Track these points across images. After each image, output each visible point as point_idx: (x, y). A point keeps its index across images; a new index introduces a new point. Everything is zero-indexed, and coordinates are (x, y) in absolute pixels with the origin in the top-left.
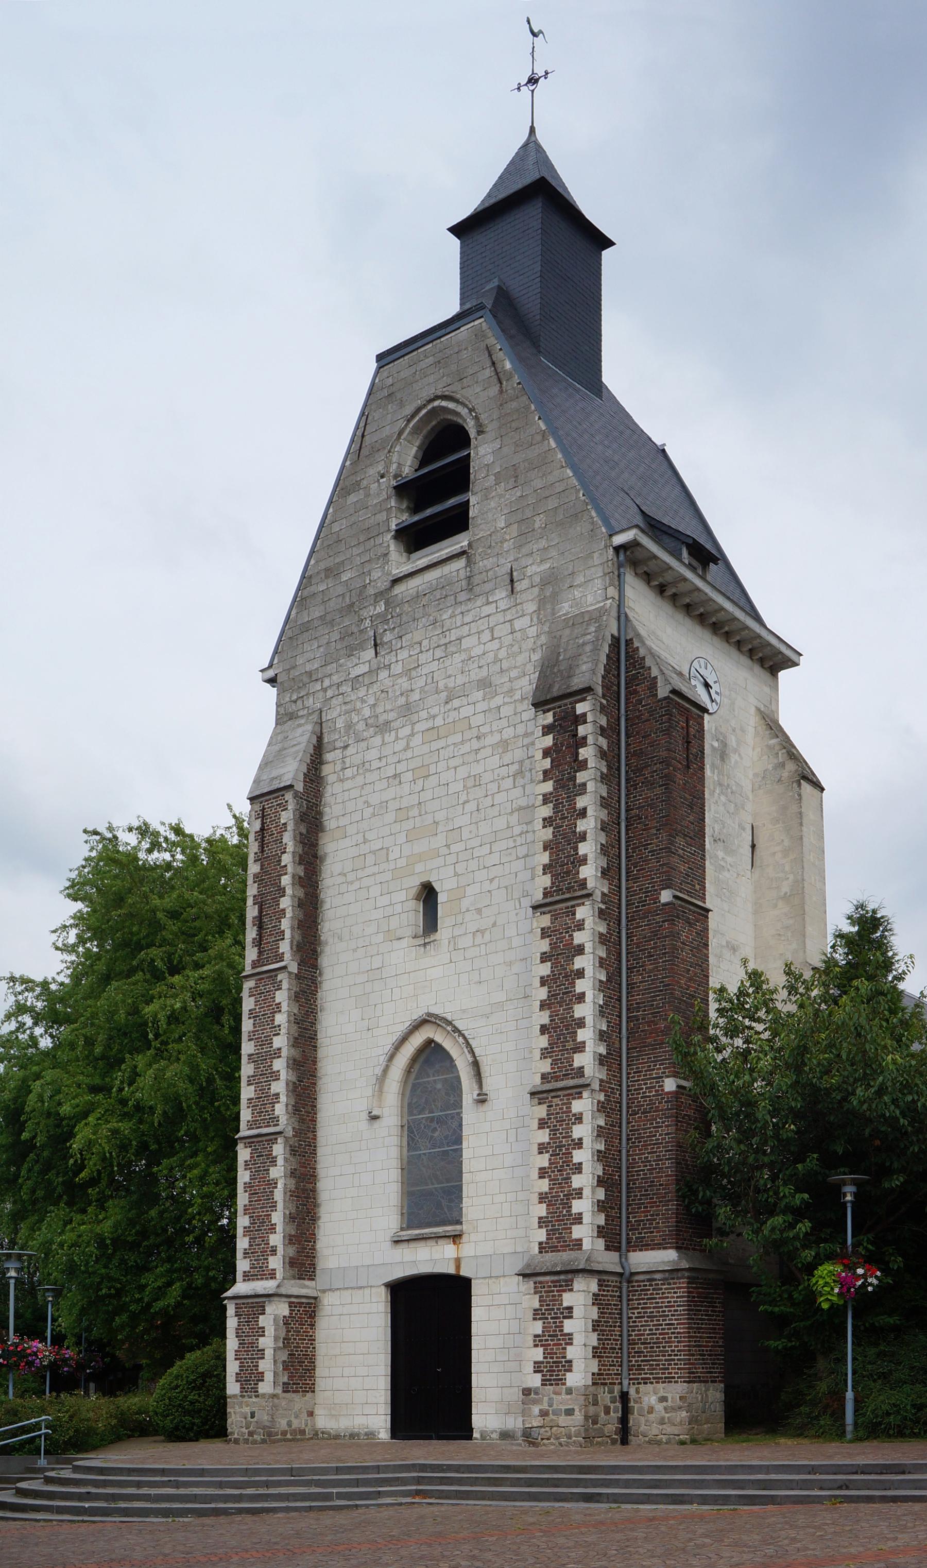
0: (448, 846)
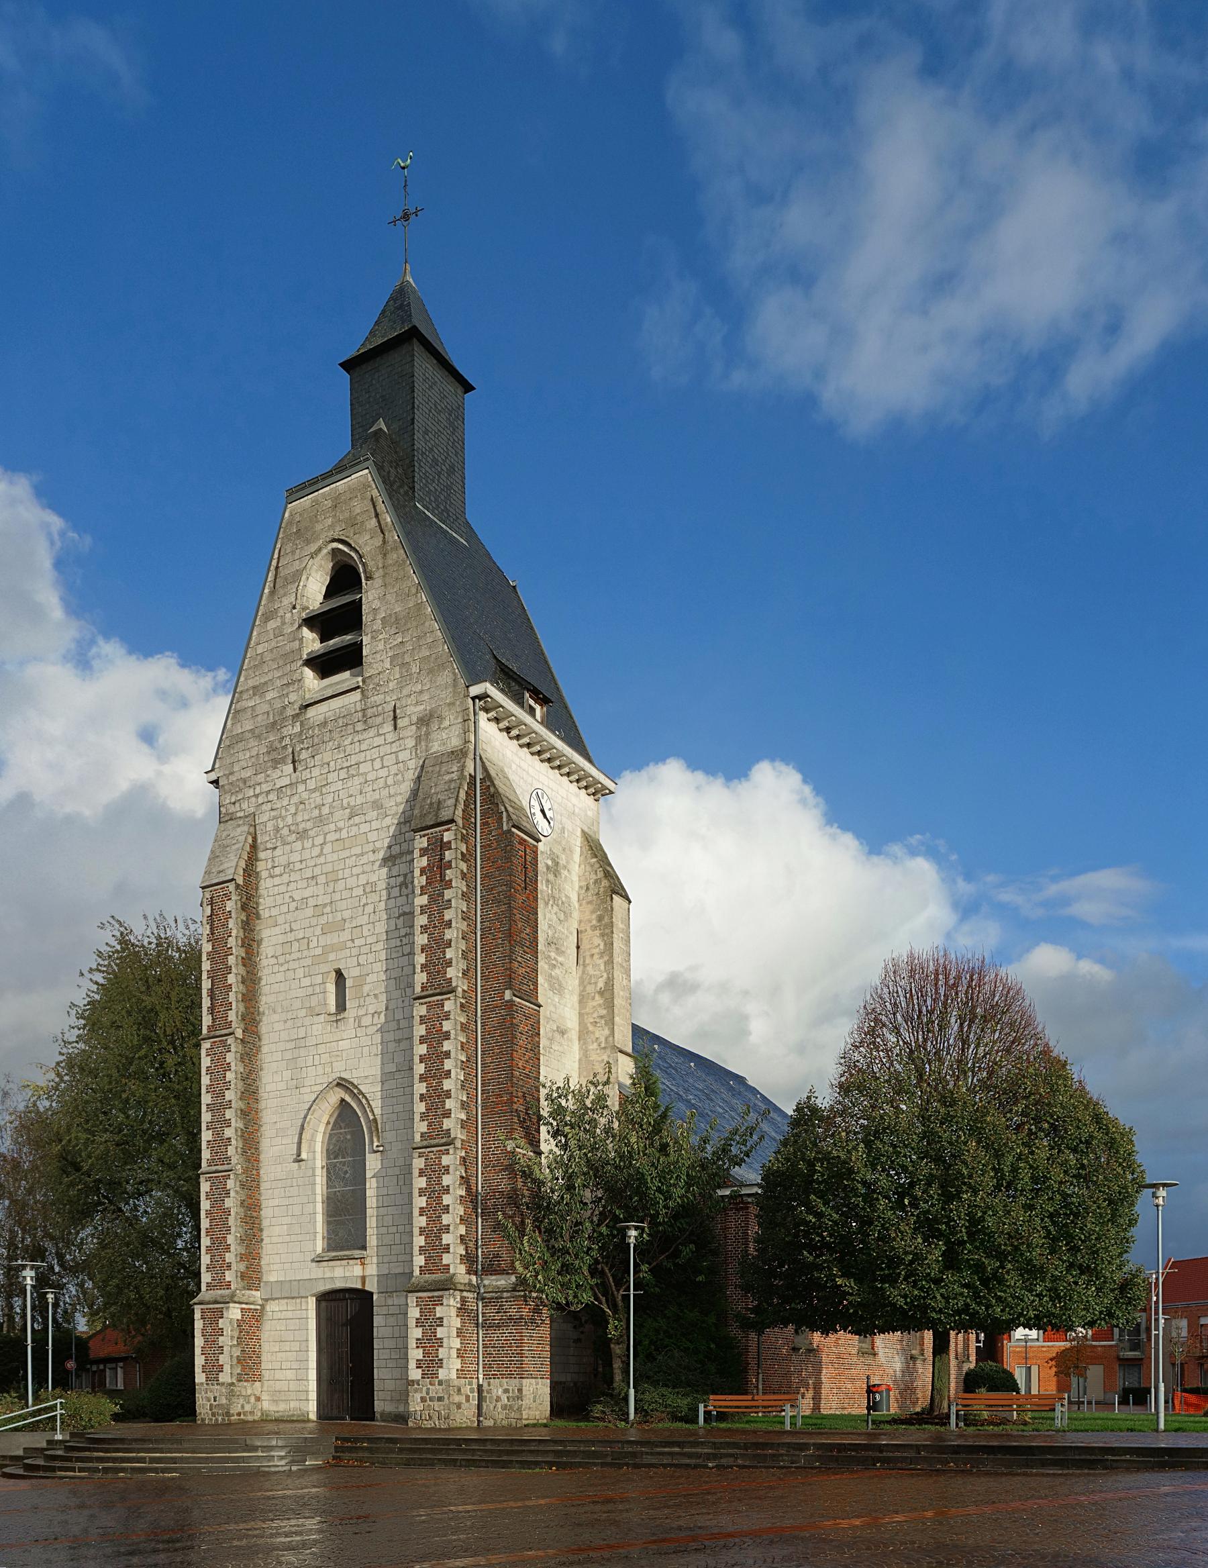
0: (352, 940)
